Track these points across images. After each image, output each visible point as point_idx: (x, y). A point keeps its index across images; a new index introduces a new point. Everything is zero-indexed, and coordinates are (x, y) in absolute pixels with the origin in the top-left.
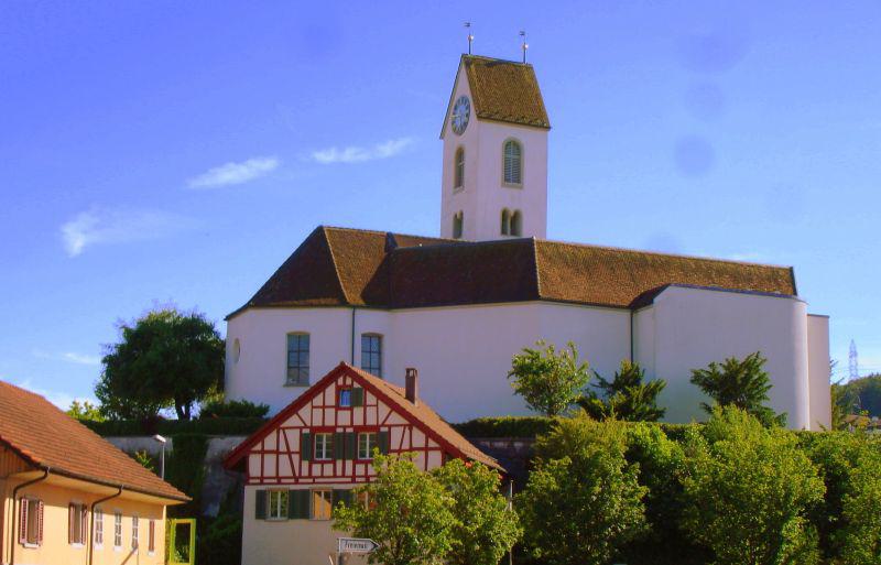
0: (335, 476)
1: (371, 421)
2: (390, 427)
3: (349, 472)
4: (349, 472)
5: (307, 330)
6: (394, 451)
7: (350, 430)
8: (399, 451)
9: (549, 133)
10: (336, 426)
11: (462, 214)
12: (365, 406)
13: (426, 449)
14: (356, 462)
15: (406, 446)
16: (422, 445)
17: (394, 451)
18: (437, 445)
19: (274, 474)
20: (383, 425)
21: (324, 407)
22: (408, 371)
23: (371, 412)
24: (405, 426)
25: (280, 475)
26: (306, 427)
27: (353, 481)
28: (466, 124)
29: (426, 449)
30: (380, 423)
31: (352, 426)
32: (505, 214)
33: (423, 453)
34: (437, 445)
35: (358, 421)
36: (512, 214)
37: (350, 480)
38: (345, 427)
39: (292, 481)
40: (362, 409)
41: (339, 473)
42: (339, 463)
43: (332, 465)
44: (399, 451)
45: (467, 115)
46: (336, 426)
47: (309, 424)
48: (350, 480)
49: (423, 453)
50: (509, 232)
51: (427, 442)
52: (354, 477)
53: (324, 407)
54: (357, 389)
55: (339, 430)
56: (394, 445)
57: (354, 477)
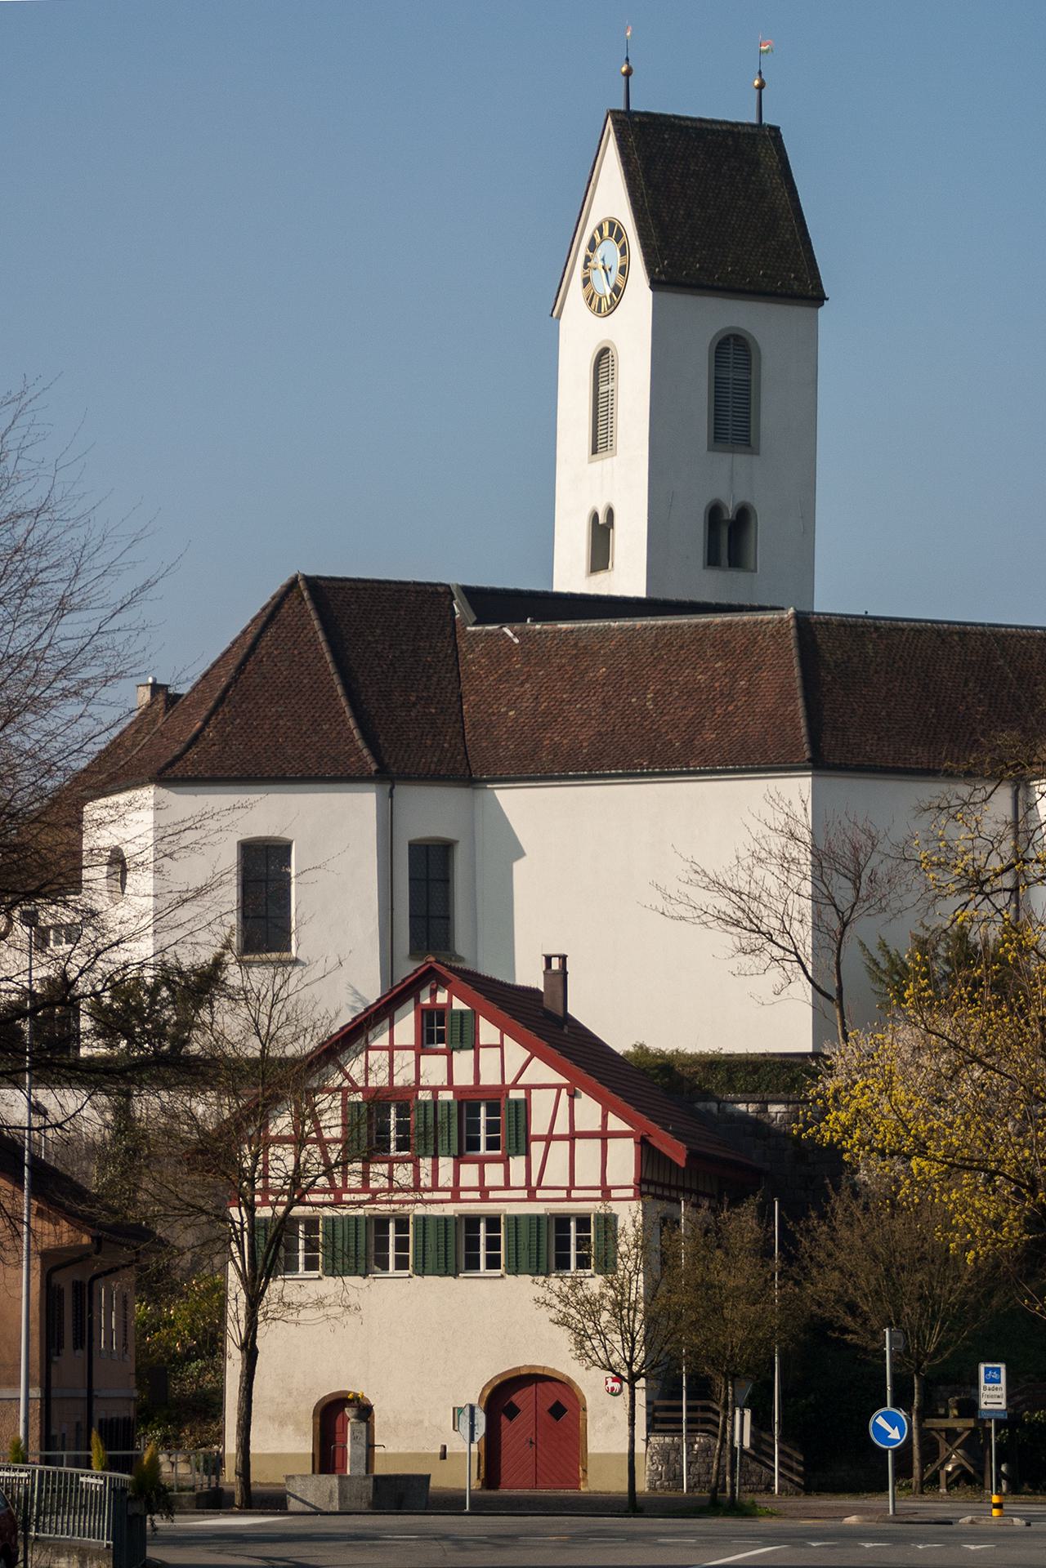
0: (417, 1188)
1: (490, 1078)
2: (528, 1088)
3: (445, 1178)
4: (445, 1178)
5: (287, 835)
6: (539, 1138)
7: (447, 1096)
8: (549, 1138)
9: (823, 312)
10: (418, 1087)
11: (610, 513)
12: (475, 1046)
13: (604, 1135)
14: (459, 1159)
15: (562, 1128)
16: (595, 1126)
17: (539, 1138)
18: (626, 1127)
19: (476, 1184)
20: (515, 1086)
21: (391, 1048)
22: (548, 959)
23: (489, 1058)
24: (559, 1087)
25: (609, 1183)
26: (355, 1089)
27: (455, 1199)
28: (618, 291)
29: (604, 1135)
30: (508, 1081)
31: (450, 1086)
32: (714, 513)
33: (385, 1054)
34: (626, 1127)
35: (464, 1078)
36: (730, 513)
37: (447, 1195)
38: (435, 1090)
39: (476, 1195)
40: (472, 1052)
41: (426, 1181)
42: (426, 1163)
43: (500, 1167)
44: (549, 1138)
45: (623, 270)
46: (418, 1087)
47: (361, 1084)
48: (447, 1195)
49: (385, 1054)
50: (674, 1403)
51: (605, 1118)
52: (456, 1191)
53: (391, 1048)
54: (462, 1013)
55: (425, 1096)
56: (538, 1126)
57: (456, 1191)
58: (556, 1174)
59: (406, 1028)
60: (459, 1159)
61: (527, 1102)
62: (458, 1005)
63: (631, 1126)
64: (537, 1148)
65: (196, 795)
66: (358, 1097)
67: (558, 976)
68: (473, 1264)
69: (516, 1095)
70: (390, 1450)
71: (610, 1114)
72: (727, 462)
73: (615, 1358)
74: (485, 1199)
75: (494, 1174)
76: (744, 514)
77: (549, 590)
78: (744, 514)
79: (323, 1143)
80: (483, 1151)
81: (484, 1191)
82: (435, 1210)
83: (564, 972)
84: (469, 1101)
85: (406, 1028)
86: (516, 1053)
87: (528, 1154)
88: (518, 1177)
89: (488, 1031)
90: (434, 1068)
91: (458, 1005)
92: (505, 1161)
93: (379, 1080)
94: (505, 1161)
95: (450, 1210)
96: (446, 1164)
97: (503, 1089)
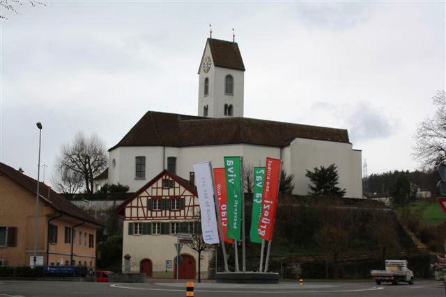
0: (162, 217)
1: (177, 194)
3: (168, 215)
4: (168, 215)
7: (168, 198)
12: (174, 188)
14: (171, 211)
22: (191, 173)
23: (177, 190)
26: (149, 196)
27: (170, 219)
31: (169, 196)
32: (226, 106)
35: (172, 194)
36: (229, 106)
38: (166, 196)
41: (164, 215)
42: (164, 212)
44: (189, 206)
52: (170, 217)
55: (164, 198)
56: (187, 204)
58: (190, 214)
59: (160, 182)
60: (171, 211)
61: (185, 199)
62: (171, 179)
63: (73, 204)
64: (186, 208)
65: (396, 172)
66: (150, 198)
67: (192, 176)
68: (154, 232)
69: (182, 197)
70: (157, 270)
71: (443, 202)
72: (228, 97)
73: (195, 246)
74: (176, 218)
75: (178, 214)
76: (231, 106)
77: (241, 116)
78: (231, 106)
79: (142, 207)
80: (176, 209)
81: (175, 217)
82: (181, 221)
83: (194, 176)
84: (173, 198)
85: (160, 182)
86: (182, 189)
87: (184, 209)
88: (183, 214)
89: (177, 185)
90: (166, 192)
91: (171, 179)
92: (180, 211)
93: (154, 194)
94: (180, 211)
95: (168, 221)
96: (168, 212)
97: (180, 196)
